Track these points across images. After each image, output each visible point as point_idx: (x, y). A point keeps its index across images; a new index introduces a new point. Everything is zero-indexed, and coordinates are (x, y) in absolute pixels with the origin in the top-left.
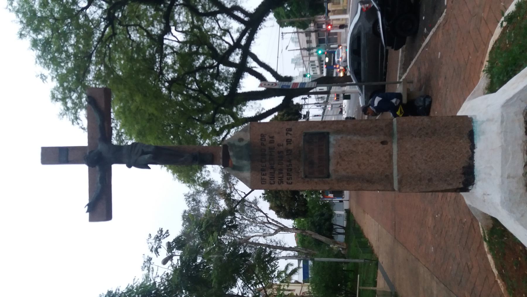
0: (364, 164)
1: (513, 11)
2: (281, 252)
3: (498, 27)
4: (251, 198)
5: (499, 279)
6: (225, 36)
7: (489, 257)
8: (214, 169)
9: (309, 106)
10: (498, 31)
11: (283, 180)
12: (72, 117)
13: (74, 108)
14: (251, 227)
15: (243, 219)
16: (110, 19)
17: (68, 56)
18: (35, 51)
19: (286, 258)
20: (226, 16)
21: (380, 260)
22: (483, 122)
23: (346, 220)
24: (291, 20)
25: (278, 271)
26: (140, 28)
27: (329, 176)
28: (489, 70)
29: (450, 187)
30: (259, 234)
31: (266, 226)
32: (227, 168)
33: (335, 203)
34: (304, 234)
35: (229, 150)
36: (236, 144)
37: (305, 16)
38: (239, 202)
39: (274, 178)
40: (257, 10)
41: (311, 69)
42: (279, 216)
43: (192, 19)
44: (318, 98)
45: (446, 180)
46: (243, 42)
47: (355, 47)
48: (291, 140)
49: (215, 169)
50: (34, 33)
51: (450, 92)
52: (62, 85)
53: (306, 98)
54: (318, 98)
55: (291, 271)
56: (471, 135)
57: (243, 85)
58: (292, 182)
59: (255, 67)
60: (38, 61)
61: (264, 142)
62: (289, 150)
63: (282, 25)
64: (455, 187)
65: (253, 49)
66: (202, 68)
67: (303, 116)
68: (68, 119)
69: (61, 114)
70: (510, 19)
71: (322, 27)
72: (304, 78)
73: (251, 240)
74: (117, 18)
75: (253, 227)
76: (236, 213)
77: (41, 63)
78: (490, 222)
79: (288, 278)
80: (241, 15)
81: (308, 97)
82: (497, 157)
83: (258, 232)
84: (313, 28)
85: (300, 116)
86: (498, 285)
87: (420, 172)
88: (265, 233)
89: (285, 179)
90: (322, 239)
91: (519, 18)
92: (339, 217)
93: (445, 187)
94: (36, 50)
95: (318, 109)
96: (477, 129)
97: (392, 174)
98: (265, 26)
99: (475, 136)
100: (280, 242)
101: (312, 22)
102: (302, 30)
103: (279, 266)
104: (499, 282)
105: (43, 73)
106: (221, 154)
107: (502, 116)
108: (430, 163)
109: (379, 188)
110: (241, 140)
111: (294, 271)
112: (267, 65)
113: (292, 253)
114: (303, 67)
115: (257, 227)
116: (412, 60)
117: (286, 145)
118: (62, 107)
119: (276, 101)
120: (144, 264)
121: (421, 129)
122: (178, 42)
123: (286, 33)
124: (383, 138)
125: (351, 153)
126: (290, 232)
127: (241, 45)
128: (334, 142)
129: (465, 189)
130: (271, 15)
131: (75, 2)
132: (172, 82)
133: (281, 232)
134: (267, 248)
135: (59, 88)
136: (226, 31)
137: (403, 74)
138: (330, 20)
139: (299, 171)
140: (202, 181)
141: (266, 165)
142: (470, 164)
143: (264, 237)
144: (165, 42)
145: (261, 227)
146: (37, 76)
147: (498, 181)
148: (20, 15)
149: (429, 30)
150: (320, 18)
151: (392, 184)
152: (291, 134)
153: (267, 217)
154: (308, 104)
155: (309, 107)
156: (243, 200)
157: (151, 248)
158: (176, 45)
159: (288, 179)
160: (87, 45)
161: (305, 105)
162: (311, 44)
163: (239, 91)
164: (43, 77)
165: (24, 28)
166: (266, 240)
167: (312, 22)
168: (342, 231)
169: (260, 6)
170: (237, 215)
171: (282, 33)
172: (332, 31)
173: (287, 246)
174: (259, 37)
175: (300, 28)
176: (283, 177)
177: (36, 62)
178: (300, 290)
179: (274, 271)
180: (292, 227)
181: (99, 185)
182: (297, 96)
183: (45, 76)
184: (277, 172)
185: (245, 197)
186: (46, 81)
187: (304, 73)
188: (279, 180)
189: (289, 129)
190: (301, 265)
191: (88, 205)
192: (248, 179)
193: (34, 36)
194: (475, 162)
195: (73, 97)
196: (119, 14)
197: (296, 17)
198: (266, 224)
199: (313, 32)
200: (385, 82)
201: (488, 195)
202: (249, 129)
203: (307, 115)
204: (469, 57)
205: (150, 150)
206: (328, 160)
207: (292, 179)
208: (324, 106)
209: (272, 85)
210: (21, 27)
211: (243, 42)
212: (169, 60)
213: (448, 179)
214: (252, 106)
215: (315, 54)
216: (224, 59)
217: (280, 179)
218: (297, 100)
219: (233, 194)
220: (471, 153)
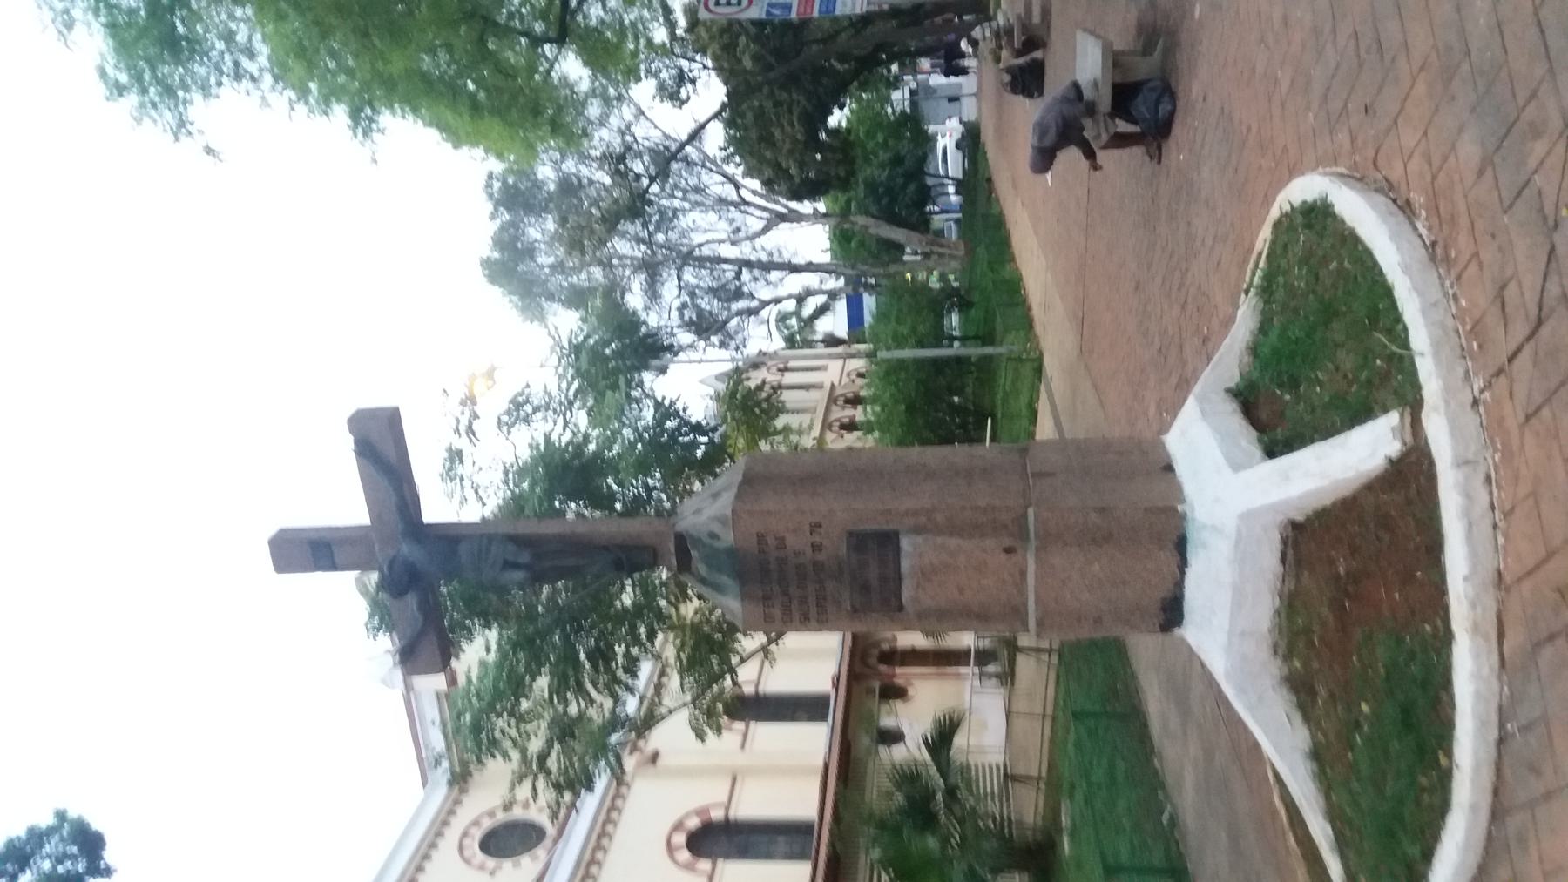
27: (901, 608)
56: (1181, 545)
79: (807, 329)
82: (1225, 598)
97: (1025, 605)
107: (1239, 533)
124: (1007, 542)
206: (899, 578)
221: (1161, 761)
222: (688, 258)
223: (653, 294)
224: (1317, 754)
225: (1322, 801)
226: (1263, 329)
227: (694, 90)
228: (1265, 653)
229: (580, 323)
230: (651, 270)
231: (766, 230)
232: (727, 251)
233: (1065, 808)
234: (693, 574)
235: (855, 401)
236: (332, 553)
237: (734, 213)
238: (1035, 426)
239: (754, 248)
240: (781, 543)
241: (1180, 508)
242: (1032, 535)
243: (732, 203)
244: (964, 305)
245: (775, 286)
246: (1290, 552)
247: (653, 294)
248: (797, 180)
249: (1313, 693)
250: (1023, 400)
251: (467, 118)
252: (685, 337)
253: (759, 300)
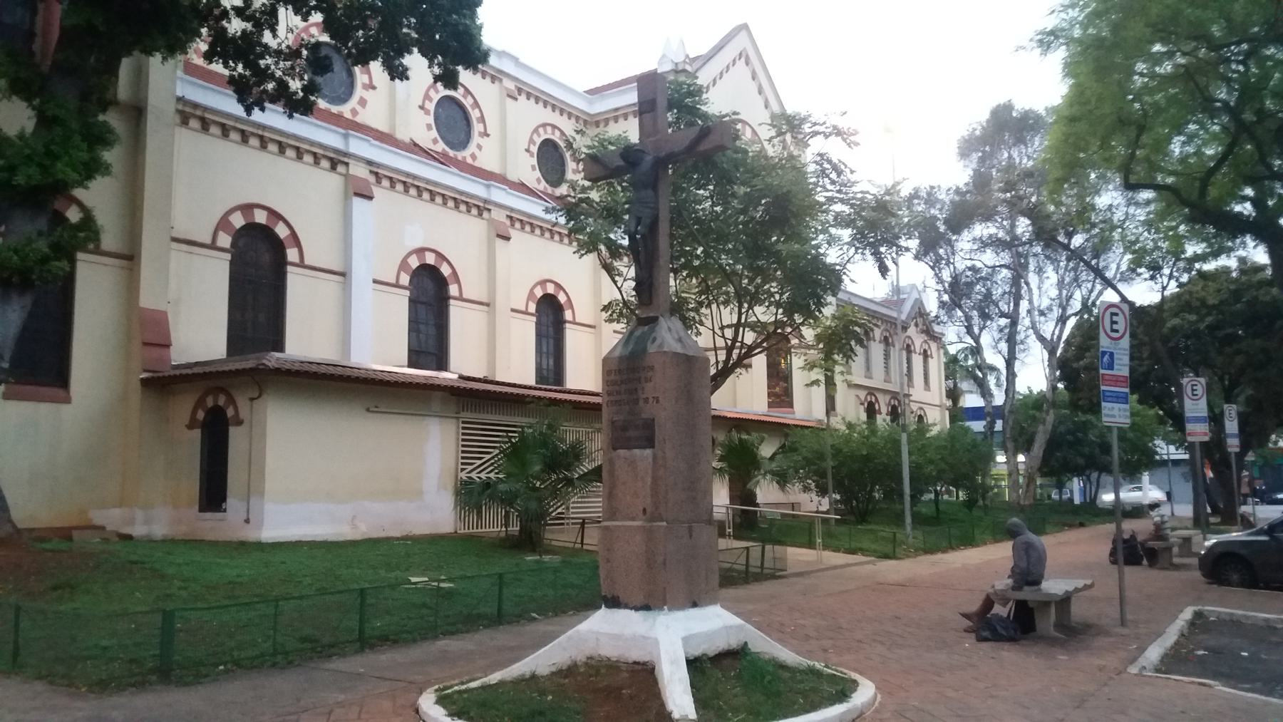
27: (615, 449)
56: (646, 608)
79: (965, 373)
90: (1035, 448)
121: (653, 551)
124: (648, 510)
128: (645, 454)
173: (1017, 365)
184: (617, 388)
221: (571, 615)
222: (1018, 273)
223: (984, 244)
224: (534, 677)
225: (509, 679)
226: (783, 667)
227: (1146, 279)
228: (588, 652)
229: (954, 188)
230: (1009, 244)
231: (1041, 339)
232: (1024, 305)
233: (557, 558)
234: (636, 327)
235: (894, 413)
237: (1056, 312)
238: (844, 553)
239: (1028, 328)
240: (648, 380)
241: (665, 607)
243: (1064, 309)
244: (970, 504)
245: (995, 347)
246: (640, 667)
247: (984, 244)
248: (1075, 365)
249: (566, 677)
250: (865, 545)
251: (1066, 113)
252: (946, 275)
253: (980, 334)
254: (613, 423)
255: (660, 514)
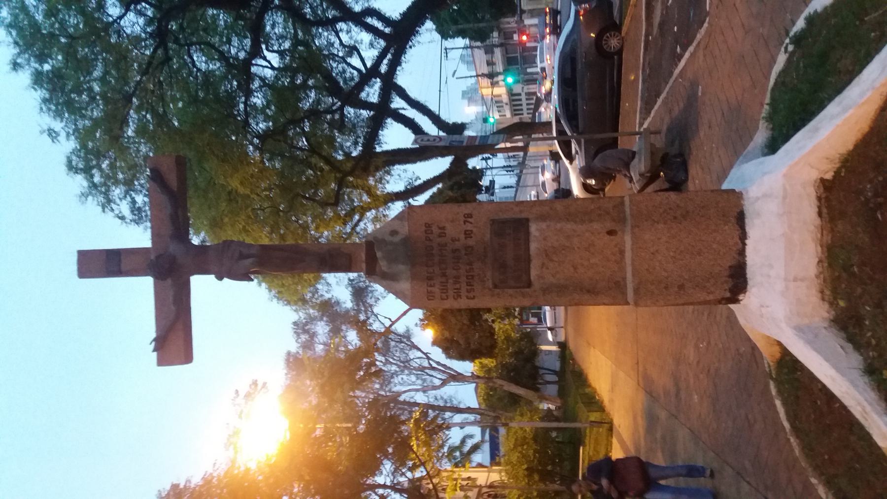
0: (582, 265)
1: (802, 28)
2: (452, 417)
3: (781, 52)
4: (400, 328)
5: (792, 436)
6: (351, 57)
7: (778, 403)
8: (338, 280)
9: (495, 171)
10: (782, 59)
11: (460, 292)
12: (101, 199)
13: (105, 184)
14: (401, 376)
15: (387, 362)
16: (161, 35)
17: (93, 99)
18: (39, 92)
19: (462, 426)
20: (350, 23)
21: (616, 422)
22: (758, 199)
23: (560, 359)
24: (460, 27)
25: (450, 447)
26: (209, 48)
27: (529, 284)
28: (770, 119)
29: (711, 297)
30: (415, 387)
31: (428, 375)
32: (374, 276)
33: (540, 332)
34: (490, 384)
35: (376, 249)
36: (386, 239)
37: (482, 20)
38: (381, 334)
39: (447, 290)
40: (405, 15)
41: (495, 108)
42: (449, 356)
43: (295, 29)
44: (509, 157)
45: (705, 287)
46: (383, 68)
47: (568, 74)
48: (471, 231)
49: (340, 280)
50: (36, 62)
51: (717, 148)
52: (84, 146)
53: (489, 158)
54: (509, 157)
55: (471, 448)
57: (385, 140)
58: (474, 296)
59: (403, 109)
60: (44, 109)
61: (429, 235)
62: (469, 247)
63: (445, 35)
64: (719, 297)
65: (402, 79)
66: (314, 114)
67: (484, 188)
68: (96, 202)
69: (83, 194)
70: (798, 40)
71: (512, 38)
72: (484, 124)
73: (402, 398)
74: (171, 31)
75: (404, 377)
76: (376, 354)
77: (49, 109)
78: (777, 349)
80: (379, 25)
81: (491, 157)
83: (414, 384)
84: (497, 39)
85: (479, 189)
86: (791, 446)
87: (666, 274)
88: (425, 385)
89: (463, 292)
91: (810, 40)
92: (548, 354)
93: (703, 296)
94: (41, 88)
95: (509, 176)
96: (749, 209)
97: (624, 279)
98: (419, 42)
99: (747, 221)
100: (450, 399)
101: (495, 29)
102: (478, 44)
103: (450, 438)
104: (792, 440)
105: (52, 127)
106: (363, 256)
107: (785, 190)
108: (681, 262)
109: (605, 301)
110: (394, 233)
111: (475, 448)
112: (422, 105)
113: (471, 417)
114: (483, 105)
115: (412, 376)
116: (658, 95)
117: (464, 239)
118: (85, 184)
119: (440, 165)
120: (228, 439)
122: (272, 68)
123: (453, 49)
124: (609, 225)
125: (563, 249)
126: (468, 382)
127: (380, 72)
128: (537, 234)
129: (736, 301)
130: (429, 24)
131: (101, 6)
132: (264, 137)
133: (452, 383)
134: (430, 411)
135: (80, 151)
136: (353, 50)
137: (645, 119)
138: (525, 26)
139: (485, 279)
140: (318, 301)
141: (434, 270)
142: (739, 261)
143: (424, 391)
144: (254, 69)
145: (419, 376)
146: (42, 132)
147: (779, 286)
148: (14, 33)
149: (684, 49)
150: (509, 23)
151: (624, 293)
152: (471, 223)
153: (429, 358)
154: (492, 168)
155: (494, 174)
156: (388, 330)
157: (239, 413)
158: (269, 73)
159: (468, 291)
160: (124, 79)
161: (487, 169)
162: (494, 67)
163: (378, 149)
164: (52, 134)
165: (19, 54)
166: (427, 396)
167: (495, 29)
168: (554, 378)
169: (409, 9)
170: (378, 357)
171: (446, 49)
172: (528, 45)
173: (462, 406)
174: (408, 61)
175: (476, 40)
176: (460, 289)
177: (41, 109)
178: (486, 478)
179: (442, 446)
180: (470, 375)
181: (173, 308)
182: (474, 155)
183: (55, 132)
184: (451, 281)
185: (391, 326)
186: (58, 140)
187: (484, 117)
188: (455, 292)
189: (468, 215)
190: (487, 437)
191: (155, 340)
192: (407, 293)
193: (37, 66)
194: (747, 259)
195: (104, 166)
196: (173, 26)
197: (468, 22)
198: (427, 371)
199: (497, 46)
200: (617, 134)
201: (767, 307)
202: (406, 215)
203: (490, 189)
204: (743, 95)
205: (253, 251)
206: (528, 260)
207: (474, 291)
208: (518, 171)
209: (434, 140)
210: (16, 52)
211: (383, 68)
212: (258, 100)
213: (708, 285)
214: (399, 175)
215: (501, 83)
216: (352, 97)
217: (455, 291)
218: (474, 163)
219: (371, 321)
220: (741, 245)
224: (871, 371)
228: (814, 298)
236: (120, 261)
242: (628, 217)
246: (825, 211)
254: (495, 286)
255: (615, 207)
